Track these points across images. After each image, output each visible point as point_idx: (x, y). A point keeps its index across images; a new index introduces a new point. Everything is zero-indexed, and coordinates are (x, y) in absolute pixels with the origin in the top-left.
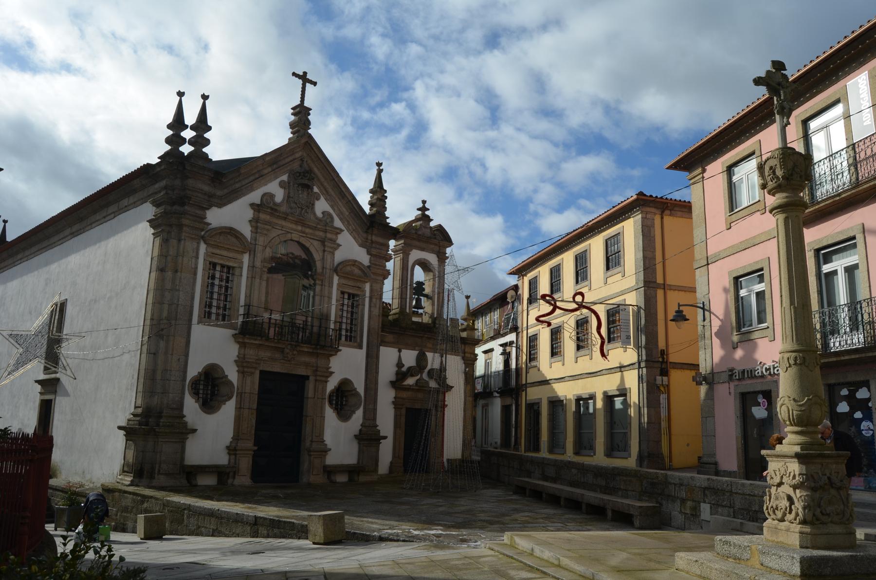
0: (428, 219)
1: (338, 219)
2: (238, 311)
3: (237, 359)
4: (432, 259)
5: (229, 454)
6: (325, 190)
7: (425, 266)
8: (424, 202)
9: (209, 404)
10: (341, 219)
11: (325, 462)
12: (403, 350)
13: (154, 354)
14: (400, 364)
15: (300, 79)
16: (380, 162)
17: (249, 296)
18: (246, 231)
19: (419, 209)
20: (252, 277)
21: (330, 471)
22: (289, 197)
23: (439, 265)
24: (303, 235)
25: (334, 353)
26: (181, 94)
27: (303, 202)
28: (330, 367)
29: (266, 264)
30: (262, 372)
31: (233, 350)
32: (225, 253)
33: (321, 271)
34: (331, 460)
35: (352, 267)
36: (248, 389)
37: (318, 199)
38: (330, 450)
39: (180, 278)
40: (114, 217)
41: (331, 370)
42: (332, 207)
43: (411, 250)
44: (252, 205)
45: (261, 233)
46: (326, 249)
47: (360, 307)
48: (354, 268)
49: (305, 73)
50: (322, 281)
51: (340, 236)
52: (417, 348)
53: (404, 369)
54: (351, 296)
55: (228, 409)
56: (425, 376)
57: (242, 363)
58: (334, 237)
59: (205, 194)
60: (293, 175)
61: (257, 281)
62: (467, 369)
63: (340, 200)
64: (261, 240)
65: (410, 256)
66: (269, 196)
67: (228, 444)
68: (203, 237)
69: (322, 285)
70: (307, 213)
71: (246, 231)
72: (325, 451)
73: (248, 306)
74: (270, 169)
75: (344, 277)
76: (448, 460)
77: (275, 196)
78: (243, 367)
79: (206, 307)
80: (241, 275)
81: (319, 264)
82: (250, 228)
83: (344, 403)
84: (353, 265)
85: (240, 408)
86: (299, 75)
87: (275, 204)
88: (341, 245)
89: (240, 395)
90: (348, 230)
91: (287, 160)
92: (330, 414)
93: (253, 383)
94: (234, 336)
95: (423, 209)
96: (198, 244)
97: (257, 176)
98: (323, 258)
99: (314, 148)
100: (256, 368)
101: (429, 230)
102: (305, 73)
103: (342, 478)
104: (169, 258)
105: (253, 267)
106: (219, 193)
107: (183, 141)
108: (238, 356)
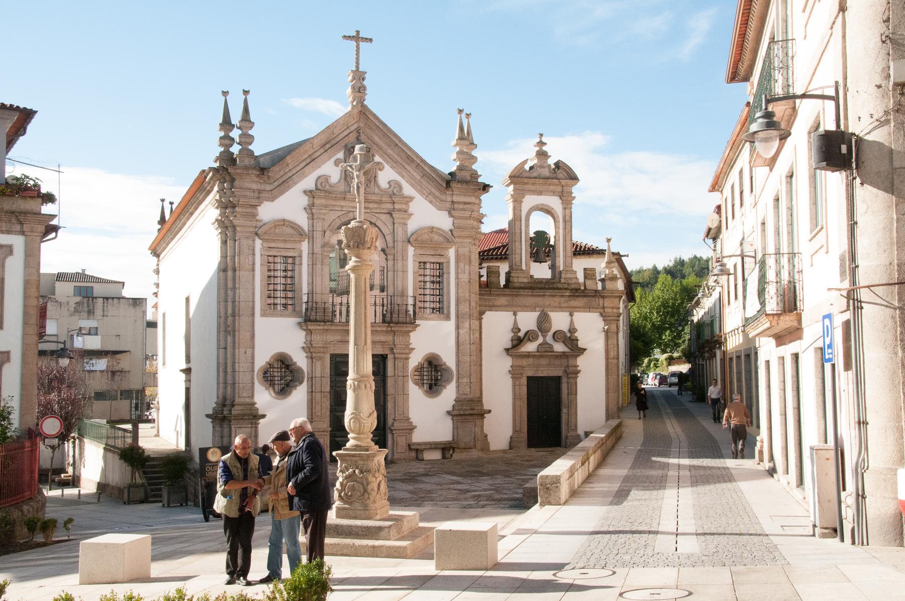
2: (301, 299)
4: (554, 202)
9: (284, 390)
10: (412, 185)
14: (516, 329)
17: (311, 283)
18: (303, 221)
26: (225, 93)
31: (300, 337)
33: (392, 244)
42: (400, 174)
43: (523, 197)
44: (308, 193)
47: (445, 276)
48: (433, 235)
49: (358, 32)
52: (537, 309)
53: (521, 334)
56: (549, 339)
57: (309, 349)
58: (404, 207)
62: (606, 327)
63: (408, 164)
64: (319, 226)
65: (523, 204)
66: (323, 180)
71: (303, 221)
72: (411, 429)
73: (311, 293)
74: (322, 151)
75: (421, 248)
82: (307, 216)
83: (439, 378)
87: (330, 186)
88: (413, 214)
89: (311, 379)
90: (422, 194)
96: (254, 240)
97: (308, 160)
99: (370, 116)
101: (547, 169)
102: (358, 32)
106: (268, 187)
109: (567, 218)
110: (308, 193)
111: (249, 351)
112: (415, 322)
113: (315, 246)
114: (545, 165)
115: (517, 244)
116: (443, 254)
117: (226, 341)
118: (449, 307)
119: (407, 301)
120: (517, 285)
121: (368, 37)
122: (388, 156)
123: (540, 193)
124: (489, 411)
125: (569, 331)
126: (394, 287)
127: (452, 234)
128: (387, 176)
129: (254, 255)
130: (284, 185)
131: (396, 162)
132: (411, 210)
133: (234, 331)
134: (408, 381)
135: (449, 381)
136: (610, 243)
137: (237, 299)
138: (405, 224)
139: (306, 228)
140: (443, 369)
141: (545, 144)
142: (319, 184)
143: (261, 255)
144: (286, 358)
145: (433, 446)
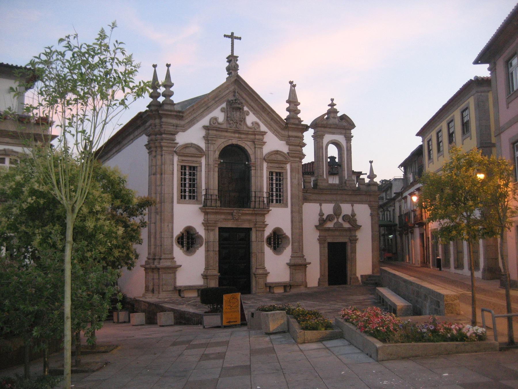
0: (336, 112)
1: (263, 125)
2: (201, 193)
3: (203, 222)
4: (341, 139)
5: (204, 279)
7: (337, 144)
8: (332, 100)
11: (266, 280)
12: (323, 204)
14: (321, 214)
15: (229, 38)
16: (292, 81)
17: (207, 183)
18: (202, 145)
19: (329, 105)
20: (208, 172)
21: (270, 287)
22: (227, 117)
23: (347, 143)
25: (266, 212)
26: (155, 66)
27: (237, 119)
28: (266, 221)
29: (216, 162)
30: (220, 229)
32: (190, 159)
33: (254, 160)
34: (270, 279)
36: (212, 239)
37: (248, 114)
38: (269, 273)
39: (164, 178)
41: (266, 223)
44: (205, 128)
46: (256, 146)
47: (285, 180)
49: (232, 33)
50: (255, 167)
51: (265, 136)
53: (325, 217)
54: (279, 174)
55: (201, 252)
56: (340, 220)
57: (207, 225)
59: (173, 126)
61: (212, 173)
67: (202, 272)
68: (175, 152)
69: (255, 170)
70: (241, 125)
71: (202, 145)
72: (266, 274)
73: (207, 190)
74: (213, 102)
76: (362, 276)
78: (208, 226)
80: (201, 171)
81: (252, 157)
84: (277, 154)
85: (208, 251)
86: (228, 36)
87: (219, 124)
89: (207, 242)
91: (224, 94)
92: (268, 251)
93: (215, 236)
94: (200, 208)
95: (332, 105)
96: (173, 156)
100: (215, 226)
102: (232, 33)
103: (279, 291)
104: (158, 167)
105: (208, 165)
106: (182, 123)
107: (159, 95)
108: (204, 220)
109: (349, 148)
111: (170, 226)
114: (336, 117)
117: (156, 218)
118: (287, 199)
120: (321, 187)
121: (239, 36)
123: (333, 133)
124: (310, 263)
128: (251, 119)
129: (173, 164)
130: (192, 123)
131: (256, 111)
132: (265, 140)
133: (161, 212)
137: (163, 192)
138: (262, 148)
139: (204, 149)
140: (283, 237)
141: (335, 105)
142: (212, 123)
143: (178, 165)
144: (192, 230)
145: (278, 285)
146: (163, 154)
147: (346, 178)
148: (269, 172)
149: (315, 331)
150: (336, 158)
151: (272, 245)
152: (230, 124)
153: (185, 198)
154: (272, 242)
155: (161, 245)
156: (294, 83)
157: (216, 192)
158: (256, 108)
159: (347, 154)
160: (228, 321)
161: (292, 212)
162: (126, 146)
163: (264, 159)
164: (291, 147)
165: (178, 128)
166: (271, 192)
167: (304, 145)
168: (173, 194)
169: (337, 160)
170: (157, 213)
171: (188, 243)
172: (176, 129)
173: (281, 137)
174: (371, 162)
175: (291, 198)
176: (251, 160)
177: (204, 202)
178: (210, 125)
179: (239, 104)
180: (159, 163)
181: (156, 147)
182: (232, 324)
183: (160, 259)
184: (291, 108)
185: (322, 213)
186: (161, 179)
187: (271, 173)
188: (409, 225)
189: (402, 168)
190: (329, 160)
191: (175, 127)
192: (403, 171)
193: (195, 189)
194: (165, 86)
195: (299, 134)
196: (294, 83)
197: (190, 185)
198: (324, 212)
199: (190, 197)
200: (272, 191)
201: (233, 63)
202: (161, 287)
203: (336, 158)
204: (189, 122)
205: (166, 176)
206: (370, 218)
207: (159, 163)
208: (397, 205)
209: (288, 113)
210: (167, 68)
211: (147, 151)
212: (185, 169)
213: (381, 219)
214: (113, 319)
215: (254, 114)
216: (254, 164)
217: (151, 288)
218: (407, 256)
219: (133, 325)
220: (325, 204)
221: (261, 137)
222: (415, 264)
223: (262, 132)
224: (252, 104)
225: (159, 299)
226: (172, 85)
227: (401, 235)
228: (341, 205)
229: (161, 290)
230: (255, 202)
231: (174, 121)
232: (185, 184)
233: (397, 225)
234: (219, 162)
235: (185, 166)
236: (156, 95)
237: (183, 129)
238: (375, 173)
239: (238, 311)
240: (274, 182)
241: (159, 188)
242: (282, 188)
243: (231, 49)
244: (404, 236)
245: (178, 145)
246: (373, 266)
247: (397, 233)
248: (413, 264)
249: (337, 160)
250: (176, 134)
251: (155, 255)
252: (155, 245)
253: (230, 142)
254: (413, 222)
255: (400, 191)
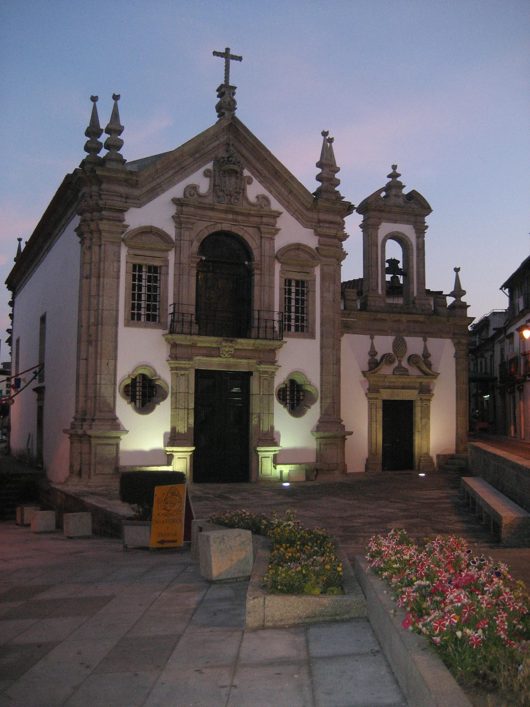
0: (401, 186)
1: (276, 201)
2: (167, 310)
6: (258, 172)
8: (394, 167)
10: (279, 201)
13: (86, 359)
14: (373, 353)
15: (222, 57)
16: (326, 131)
17: (177, 294)
18: (170, 230)
19: (389, 176)
22: (215, 186)
23: (418, 237)
24: (235, 223)
26: (94, 99)
27: (231, 189)
29: (193, 260)
32: (148, 253)
33: (259, 259)
35: (297, 251)
37: (250, 182)
39: (103, 284)
40: (64, 230)
44: (176, 202)
45: (185, 228)
46: (263, 235)
47: (311, 294)
48: (299, 252)
49: (228, 50)
53: (378, 358)
54: (300, 283)
59: (122, 196)
60: (218, 163)
65: (379, 231)
68: (123, 240)
69: (261, 274)
71: (170, 230)
76: (438, 456)
77: (199, 187)
79: (285, 294)
80: (167, 274)
81: (256, 253)
83: (301, 398)
87: (200, 196)
88: (280, 229)
89: (175, 395)
91: (210, 147)
95: (394, 176)
96: (119, 246)
98: (261, 246)
102: (228, 50)
104: (93, 264)
105: (180, 263)
106: (136, 192)
109: (420, 246)
110: (176, 202)
111: (112, 363)
112: (282, 339)
113: (182, 256)
115: (374, 269)
116: (309, 271)
117: (88, 351)
119: (273, 316)
121: (239, 55)
122: (256, 170)
123: (395, 221)
125: (423, 355)
126: (261, 303)
127: (318, 253)
129: (119, 261)
132: (278, 226)
133: (97, 341)
134: (273, 400)
135: (313, 401)
136: (459, 273)
138: (272, 239)
139: (173, 236)
141: (399, 175)
143: (127, 262)
146: (103, 243)
147: (415, 294)
148: (283, 280)
149: (293, 599)
150: (399, 262)
151: (288, 401)
152: (219, 197)
153: (139, 319)
154: (288, 397)
155: (95, 397)
156: (330, 136)
157: (192, 310)
158: (265, 172)
159: (418, 256)
160: (161, 539)
161: (322, 347)
162: (57, 237)
163: (276, 257)
164: (323, 239)
165: (128, 201)
166: (287, 314)
167: (345, 237)
168: (117, 311)
169: (400, 266)
170: (89, 342)
171: (144, 395)
172: (126, 202)
173: (306, 223)
174: (457, 270)
175: (322, 324)
176: (254, 258)
177: (171, 325)
178: (184, 196)
179: (234, 164)
180: (95, 258)
181: (91, 232)
182: (166, 545)
183: (93, 420)
184: (324, 175)
185: (375, 351)
186: (98, 285)
187: (288, 282)
188: (518, 377)
189: (507, 291)
190: (387, 265)
191: (124, 200)
192: (508, 294)
193: (157, 303)
194: (108, 131)
195: (338, 219)
196: (330, 136)
197: (149, 296)
198: (377, 349)
199: (149, 318)
200: (290, 311)
201: (227, 99)
202: (92, 467)
203: (399, 262)
204: (148, 192)
205: (106, 280)
206: (454, 359)
207: (95, 258)
208: (497, 348)
209: (319, 184)
210: (113, 102)
211: (79, 239)
212: (140, 270)
213: (472, 369)
214: (15, 519)
215: (260, 182)
216: (258, 265)
217: (76, 468)
218: (512, 428)
219: (35, 533)
220: (381, 337)
221: (271, 221)
222: (524, 439)
223: (274, 212)
224: (258, 166)
225: (89, 487)
226: (120, 131)
227: (503, 398)
228: (406, 338)
229: (92, 473)
230: (259, 328)
231: (123, 190)
232: (140, 296)
233: (496, 378)
234: (198, 260)
235: (140, 267)
236: (94, 145)
237: (137, 202)
238: (463, 288)
239: (180, 521)
240: (293, 296)
241: (94, 301)
242: (306, 307)
243: (224, 76)
244: (507, 396)
245: (128, 230)
246: (457, 438)
247: (497, 392)
248: (521, 439)
249: (400, 266)
250: (126, 211)
251: (85, 413)
252: (86, 396)
253: (218, 228)
254: (522, 373)
255: (503, 326)
